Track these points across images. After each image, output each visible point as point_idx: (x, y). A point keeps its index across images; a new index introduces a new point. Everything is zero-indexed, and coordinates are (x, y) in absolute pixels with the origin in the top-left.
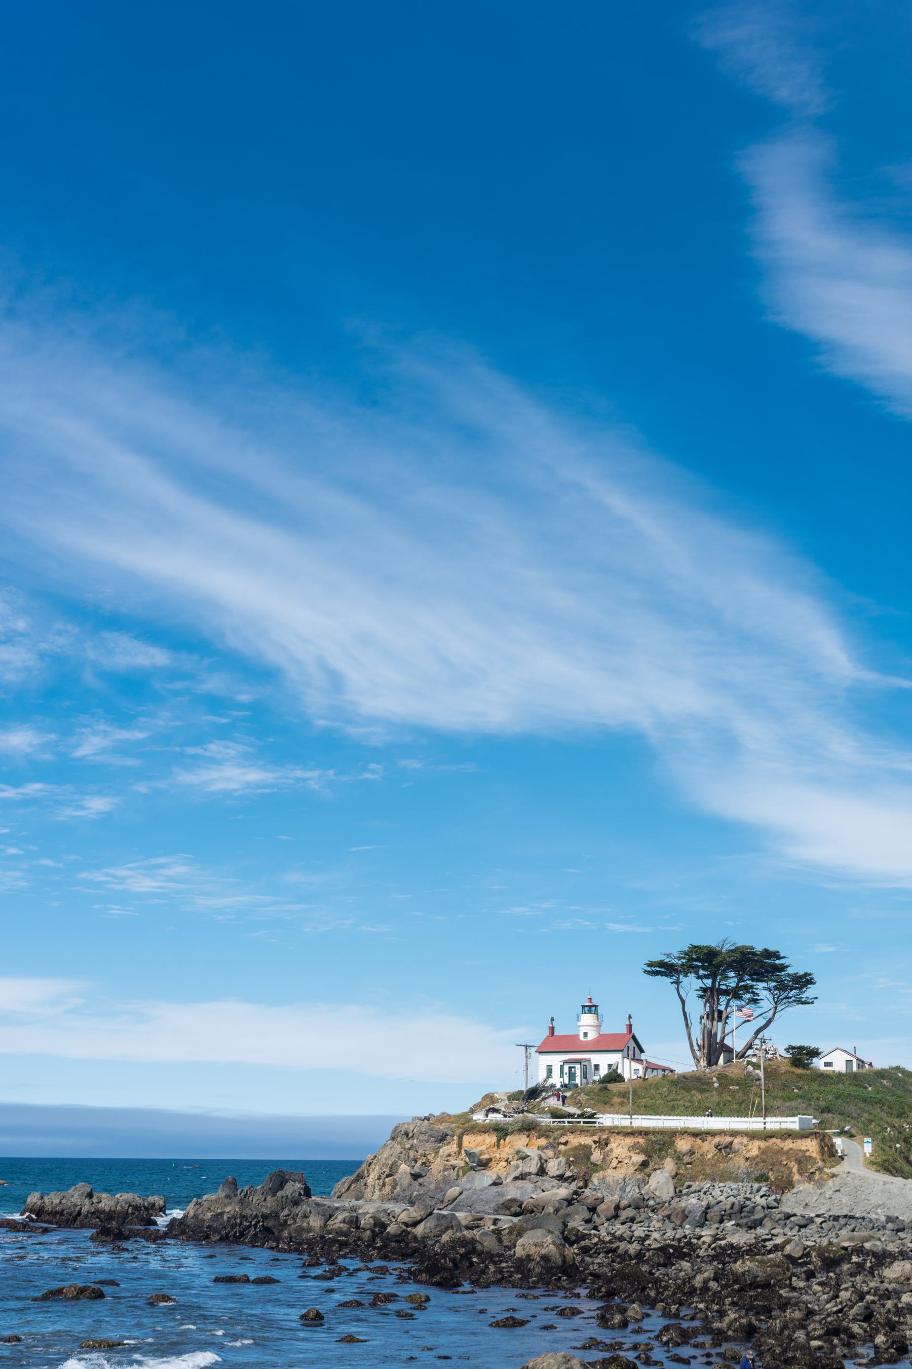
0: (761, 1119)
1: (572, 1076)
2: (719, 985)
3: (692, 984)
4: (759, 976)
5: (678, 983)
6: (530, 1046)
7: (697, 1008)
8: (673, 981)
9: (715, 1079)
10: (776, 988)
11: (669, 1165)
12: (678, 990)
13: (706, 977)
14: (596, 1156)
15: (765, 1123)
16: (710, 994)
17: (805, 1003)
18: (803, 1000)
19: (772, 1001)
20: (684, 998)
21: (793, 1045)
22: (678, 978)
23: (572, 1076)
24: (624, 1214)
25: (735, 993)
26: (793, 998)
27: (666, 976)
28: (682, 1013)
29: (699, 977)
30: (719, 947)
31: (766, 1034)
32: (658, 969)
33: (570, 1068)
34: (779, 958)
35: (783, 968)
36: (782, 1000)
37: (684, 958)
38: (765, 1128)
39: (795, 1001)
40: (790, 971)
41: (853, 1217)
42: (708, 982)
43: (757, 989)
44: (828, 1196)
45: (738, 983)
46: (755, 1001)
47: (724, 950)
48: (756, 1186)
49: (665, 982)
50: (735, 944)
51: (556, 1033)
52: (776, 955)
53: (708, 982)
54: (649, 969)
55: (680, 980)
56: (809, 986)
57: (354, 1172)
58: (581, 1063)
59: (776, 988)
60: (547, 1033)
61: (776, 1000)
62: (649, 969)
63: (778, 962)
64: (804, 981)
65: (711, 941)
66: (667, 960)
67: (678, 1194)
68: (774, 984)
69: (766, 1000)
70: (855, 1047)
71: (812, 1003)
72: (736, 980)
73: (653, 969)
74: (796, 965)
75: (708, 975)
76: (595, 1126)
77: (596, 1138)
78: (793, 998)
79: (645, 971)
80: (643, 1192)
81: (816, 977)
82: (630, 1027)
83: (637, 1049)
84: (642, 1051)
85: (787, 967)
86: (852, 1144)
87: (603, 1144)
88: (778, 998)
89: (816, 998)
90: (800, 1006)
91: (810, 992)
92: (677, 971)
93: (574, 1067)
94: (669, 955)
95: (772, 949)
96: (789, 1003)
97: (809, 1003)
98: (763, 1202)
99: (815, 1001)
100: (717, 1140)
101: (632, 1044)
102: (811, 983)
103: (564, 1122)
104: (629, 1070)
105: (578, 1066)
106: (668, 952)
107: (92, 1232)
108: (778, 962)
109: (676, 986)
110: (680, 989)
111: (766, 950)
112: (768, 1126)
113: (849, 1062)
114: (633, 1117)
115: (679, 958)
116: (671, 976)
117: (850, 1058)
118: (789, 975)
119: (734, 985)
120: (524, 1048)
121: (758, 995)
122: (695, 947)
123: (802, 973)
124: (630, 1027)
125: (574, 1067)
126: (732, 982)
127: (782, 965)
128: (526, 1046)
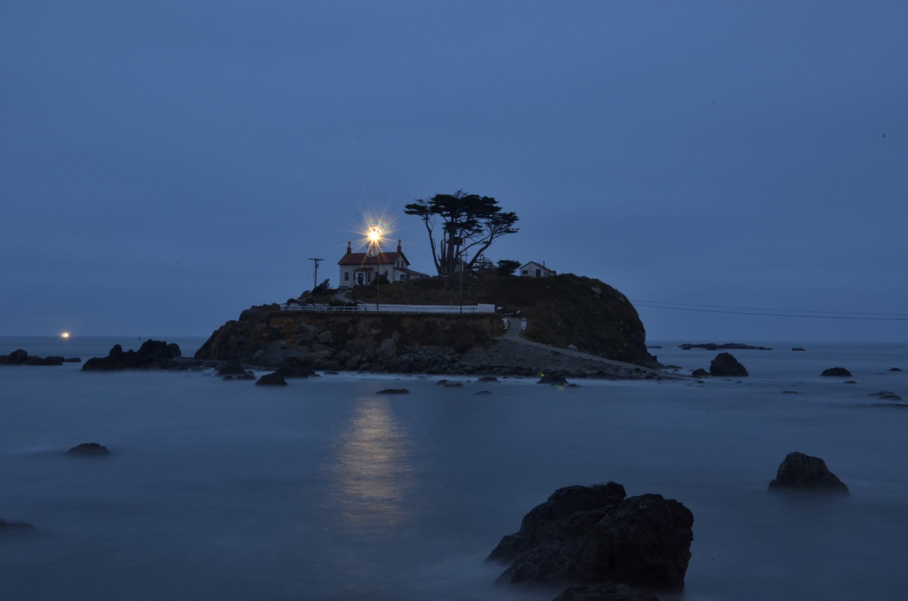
0: (459, 307)
1: (360, 280)
2: (456, 221)
3: (438, 221)
5: (427, 219)
6: (318, 260)
7: (440, 235)
8: (424, 218)
9: (446, 281)
10: (493, 223)
11: (396, 335)
12: (427, 223)
14: (350, 330)
15: (461, 309)
16: (450, 228)
17: (512, 232)
18: (511, 230)
19: (490, 232)
20: (431, 229)
21: (503, 259)
22: (427, 216)
23: (360, 280)
25: (468, 225)
26: (504, 230)
27: (419, 214)
28: (429, 239)
29: (444, 216)
30: (455, 195)
31: (484, 252)
32: (413, 210)
33: (359, 274)
34: (495, 202)
36: (497, 230)
37: (433, 203)
38: (461, 312)
39: (504, 231)
40: (502, 211)
41: (503, 367)
42: (449, 219)
43: (479, 222)
44: (612, 367)
45: (468, 220)
46: (480, 231)
47: (459, 198)
49: (418, 219)
50: (466, 194)
51: (353, 252)
52: (492, 201)
53: (449, 219)
54: (407, 210)
55: (428, 217)
56: (515, 221)
58: (366, 271)
59: (493, 223)
60: (346, 252)
61: (492, 230)
62: (407, 210)
64: (510, 218)
66: (418, 204)
68: (491, 220)
69: (486, 231)
70: (544, 262)
71: (516, 232)
72: (466, 217)
73: (411, 210)
74: (506, 208)
75: (449, 214)
76: (352, 312)
78: (504, 230)
79: (407, 213)
80: (376, 352)
81: (518, 215)
82: (399, 248)
83: (404, 262)
84: (408, 264)
85: (501, 208)
86: (514, 321)
88: (494, 229)
89: (518, 229)
90: (508, 234)
91: (514, 226)
92: (427, 212)
93: (362, 274)
94: (421, 201)
95: (489, 196)
96: (502, 232)
97: (514, 232)
98: (449, 358)
99: (518, 230)
101: (400, 259)
102: (516, 220)
103: (352, 309)
104: (394, 276)
105: (364, 273)
106: (419, 199)
109: (425, 221)
110: (428, 223)
111: (485, 198)
112: (464, 311)
113: (545, 273)
114: (379, 305)
115: (430, 203)
116: (421, 215)
117: (539, 268)
120: (314, 261)
121: (481, 227)
122: (439, 195)
123: (508, 212)
124: (399, 248)
125: (362, 274)
126: (463, 219)
127: (497, 207)
128: (316, 260)
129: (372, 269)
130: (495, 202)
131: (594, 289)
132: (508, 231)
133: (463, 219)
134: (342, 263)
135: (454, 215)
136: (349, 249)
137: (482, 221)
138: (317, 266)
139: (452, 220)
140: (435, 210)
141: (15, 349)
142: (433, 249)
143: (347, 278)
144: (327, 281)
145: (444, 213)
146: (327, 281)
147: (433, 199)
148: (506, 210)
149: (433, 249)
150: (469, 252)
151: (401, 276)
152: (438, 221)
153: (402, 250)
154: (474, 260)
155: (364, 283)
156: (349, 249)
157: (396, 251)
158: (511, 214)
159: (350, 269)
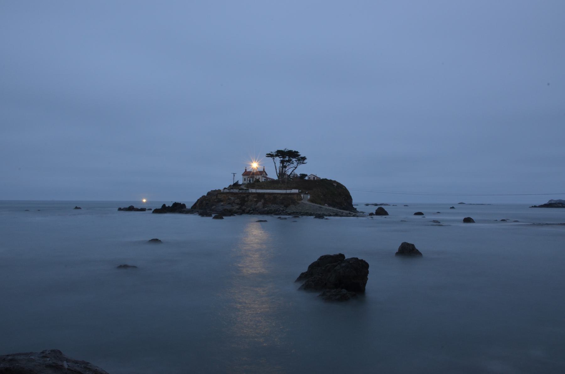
0: (285, 191)
1: (250, 181)
3: (278, 159)
4: (294, 157)
5: (274, 159)
10: (298, 160)
13: (281, 157)
14: (246, 199)
16: (282, 162)
20: (275, 162)
23: (250, 181)
24: (250, 212)
29: (280, 158)
34: (298, 153)
35: (300, 155)
40: (301, 156)
42: (282, 159)
46: (293, 163)
48: (281, 205)
49: (271, 159)
52: (297, 152)
53: (282, 159)
57: (321, 205)
63: (298, 154)
64: (304, 158)
65: (282, 149)
67: (264, 207)
72: (288, 158)
77: (246, 195)
79: (267, 156)
82: (264, 169)
84: (267, 175)
86: (305, 196)
87: (248, 196)
90: (303, 164)
91: (305, 161)
92: (274, 156)
94: (272, 152)
100: (274, 195)
101: (264, 173)
105: (251, 178)
106: (271, 151)
107: (314, 217)
108: (298, 154)
111: (295, 151)
112: (287, 192)
115: (275, 153)
118: (300, 157)
119: (288, 159)
121: (293, 162)
124: (264, 169)
126: (287, 159)
128: (234, 174)
129: (254, 177)
130: (298, 153)
131: (334, 184)
132: (303, 163)
133: (287, 159)
134: (243, 175)
135: (284, 157)
136: (246, 170)
137: (294, 160)
138: (234, 176)
139: (283, 159)
140: (277, 155)
141: (130, 205)
142: (276, 170)
143: (245, 180)
144: (238, 181)
145: (280, 157)
146: (238, 181)
147: (276, 152)
148: (302, 155)
149: (276, 170)
150: (289, 171)
151: (265, 179)
152: (278, 159)
153: (265, 170)
154: (291, 174)
155: (251, 182)
156: (246, 170)
157: (263, 170)
158: (304, 157)
159: (246, 177)
